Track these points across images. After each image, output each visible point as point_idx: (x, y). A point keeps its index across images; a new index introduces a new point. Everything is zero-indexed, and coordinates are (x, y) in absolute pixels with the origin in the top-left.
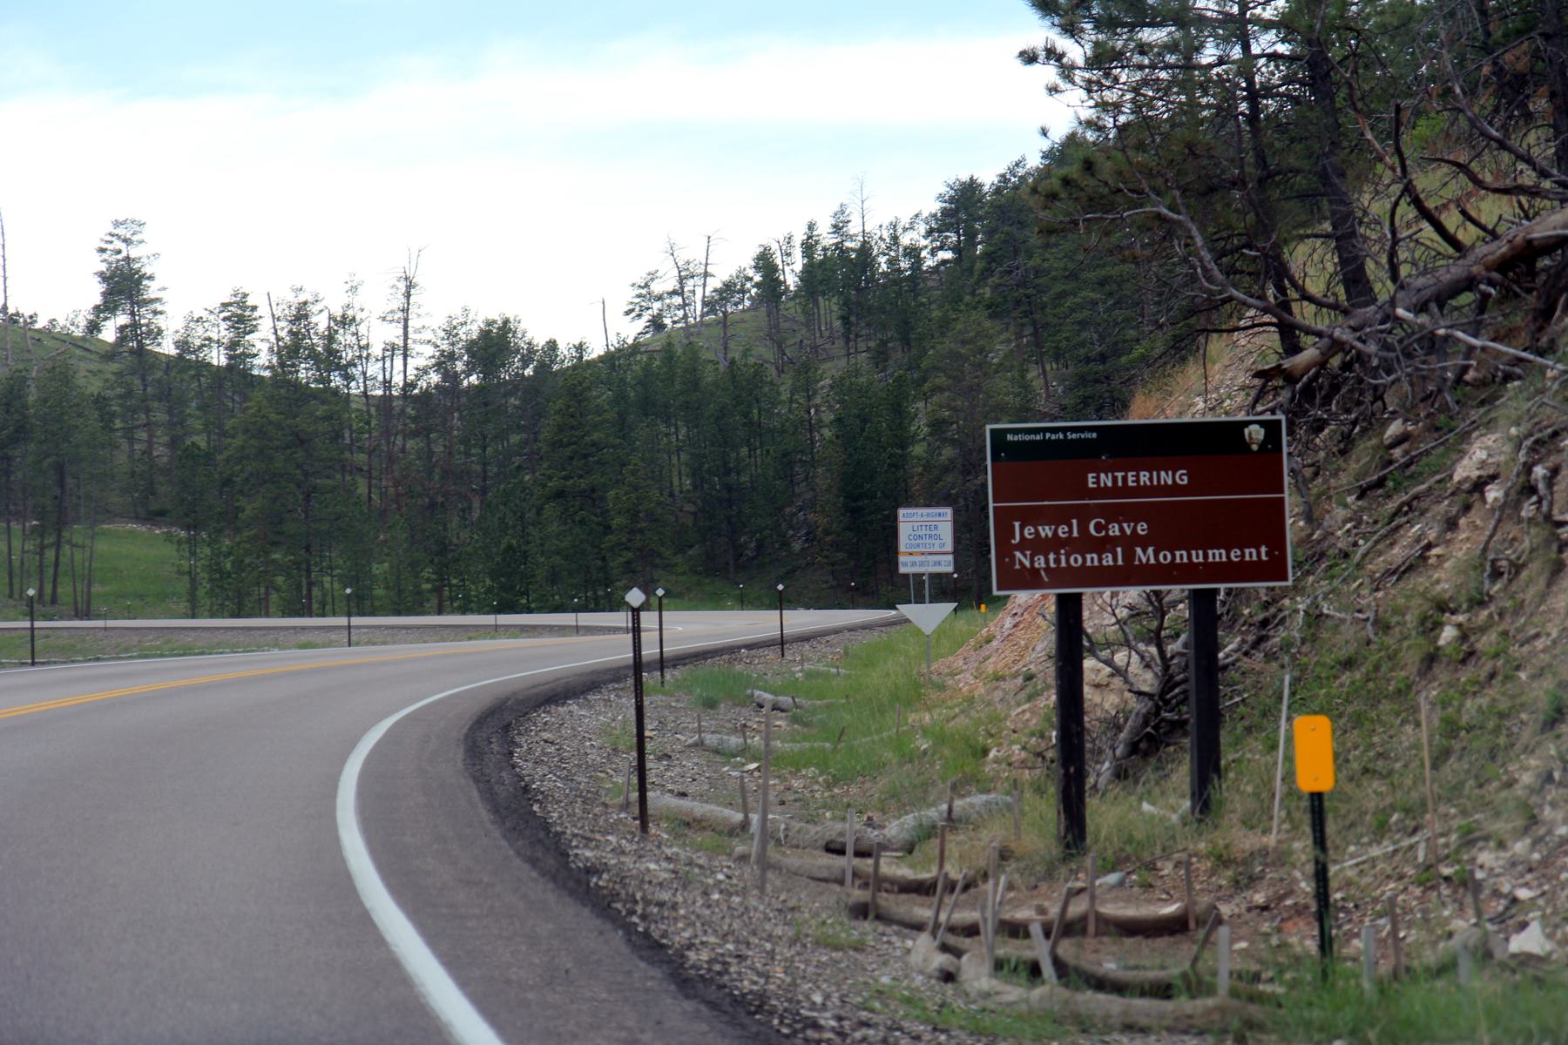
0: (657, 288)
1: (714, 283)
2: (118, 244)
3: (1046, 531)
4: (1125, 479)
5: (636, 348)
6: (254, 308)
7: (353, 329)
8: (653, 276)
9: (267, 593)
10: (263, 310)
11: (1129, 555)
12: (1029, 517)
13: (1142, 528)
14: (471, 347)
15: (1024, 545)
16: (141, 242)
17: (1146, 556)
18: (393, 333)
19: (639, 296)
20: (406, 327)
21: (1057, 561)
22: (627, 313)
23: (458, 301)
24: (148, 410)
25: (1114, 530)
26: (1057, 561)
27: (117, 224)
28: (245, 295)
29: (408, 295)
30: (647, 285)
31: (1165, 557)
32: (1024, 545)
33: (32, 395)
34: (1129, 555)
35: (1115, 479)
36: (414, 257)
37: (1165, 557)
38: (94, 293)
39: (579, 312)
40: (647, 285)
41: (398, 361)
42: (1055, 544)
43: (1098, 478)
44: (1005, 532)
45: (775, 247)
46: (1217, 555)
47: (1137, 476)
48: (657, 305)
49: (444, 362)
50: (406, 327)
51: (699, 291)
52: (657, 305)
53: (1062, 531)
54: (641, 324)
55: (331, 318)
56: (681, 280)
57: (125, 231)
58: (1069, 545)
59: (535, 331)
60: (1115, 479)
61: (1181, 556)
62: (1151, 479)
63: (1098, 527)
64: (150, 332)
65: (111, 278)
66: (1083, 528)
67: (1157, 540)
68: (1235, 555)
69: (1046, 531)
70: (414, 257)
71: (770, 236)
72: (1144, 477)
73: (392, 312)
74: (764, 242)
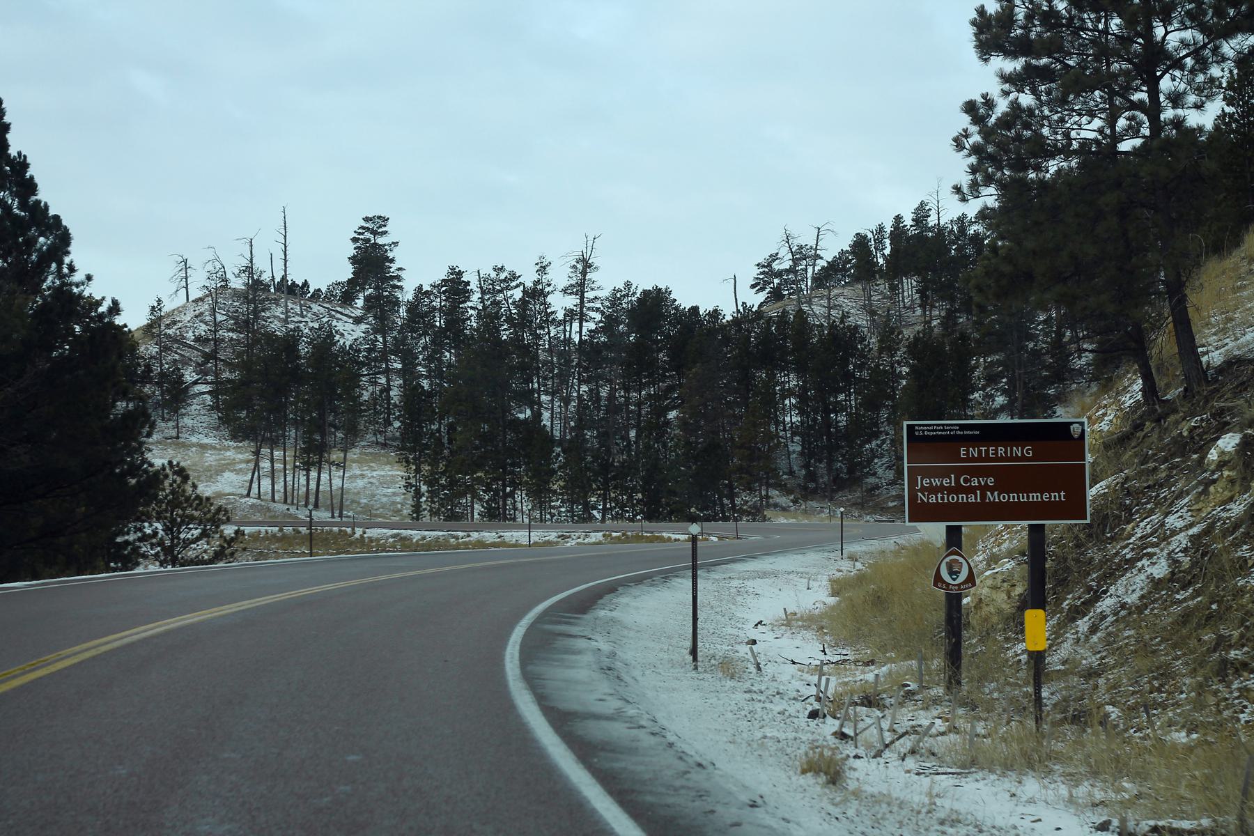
0: (776, 266)
1: (821, 263)
2: (368, 235)
3: (936, 482)
4: (987, 452)
5: (759, 314)
6: (468, 283)
7: (541, 299)
8: (774, 257)
9: (472, 502)
10: (474, 286)
11: (983, 496)
12: (928, 473)
13: (991, 481)
14: (632, 312)
15: (923, 489)
16: (385, 232)
17: (993, 497)
18: (572, 301)
19: (762, 273)
20: (582, 298)
21: (942, 498)
22: (753, 286)
23: (623, 271)
24: (387, 361)
25: (975, 482)
26: (942, 498)
27: (367, 219)
28: (460, 273)
29: (584, 273)
30: (769, 265)
31: (1004, 498)
32: (923, 489)
33: (303, 349)
34: (983, 496)
35: (980, 452)
36: (590, 243)
37: (1004, 498)
38: (346, 272)
39: (715, 282)
40: (769, 265)
41: (576, 326)
42: (941, 489)
43: (968, 451)
44: (912, 482)
45: (870, 236)
46: (1035, 497)
47: (996, 451)
48: (776, 281)
49: (610, 322)
50: (582, 298)
51: (810, 270)
52: (776, 281)
53: (946, 482)
54: (762, 296)
55: (525, 292)
56: (795, 261)
57: (377, 224)
58: (951, 490)
59: (684, 299)
60: (980, 452)
61: (1013, 497)
62: (1006, 452)
63: (966, 481)
64: (390, 302)
65: (362, 259)
66: (957, 481)
67: (1000, 487)
68: (1045, 497)
69: (936, 482)
70: (590, 243)
71: (867, 227)
72: (1001, 451)
73: (571, 285)
74: (862, 232)
